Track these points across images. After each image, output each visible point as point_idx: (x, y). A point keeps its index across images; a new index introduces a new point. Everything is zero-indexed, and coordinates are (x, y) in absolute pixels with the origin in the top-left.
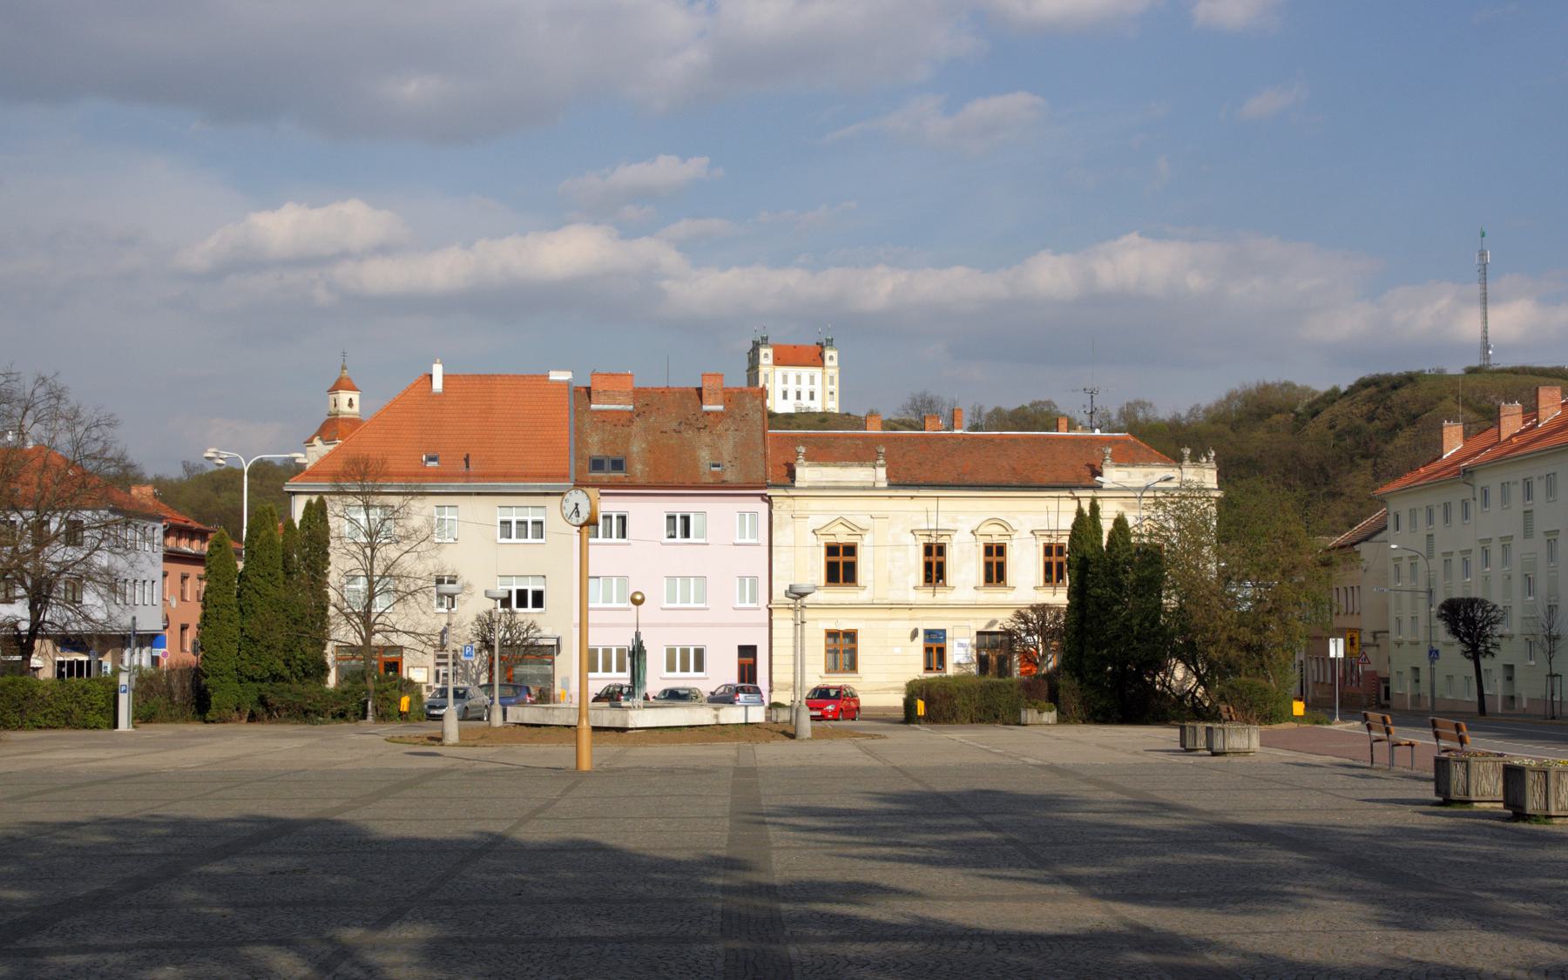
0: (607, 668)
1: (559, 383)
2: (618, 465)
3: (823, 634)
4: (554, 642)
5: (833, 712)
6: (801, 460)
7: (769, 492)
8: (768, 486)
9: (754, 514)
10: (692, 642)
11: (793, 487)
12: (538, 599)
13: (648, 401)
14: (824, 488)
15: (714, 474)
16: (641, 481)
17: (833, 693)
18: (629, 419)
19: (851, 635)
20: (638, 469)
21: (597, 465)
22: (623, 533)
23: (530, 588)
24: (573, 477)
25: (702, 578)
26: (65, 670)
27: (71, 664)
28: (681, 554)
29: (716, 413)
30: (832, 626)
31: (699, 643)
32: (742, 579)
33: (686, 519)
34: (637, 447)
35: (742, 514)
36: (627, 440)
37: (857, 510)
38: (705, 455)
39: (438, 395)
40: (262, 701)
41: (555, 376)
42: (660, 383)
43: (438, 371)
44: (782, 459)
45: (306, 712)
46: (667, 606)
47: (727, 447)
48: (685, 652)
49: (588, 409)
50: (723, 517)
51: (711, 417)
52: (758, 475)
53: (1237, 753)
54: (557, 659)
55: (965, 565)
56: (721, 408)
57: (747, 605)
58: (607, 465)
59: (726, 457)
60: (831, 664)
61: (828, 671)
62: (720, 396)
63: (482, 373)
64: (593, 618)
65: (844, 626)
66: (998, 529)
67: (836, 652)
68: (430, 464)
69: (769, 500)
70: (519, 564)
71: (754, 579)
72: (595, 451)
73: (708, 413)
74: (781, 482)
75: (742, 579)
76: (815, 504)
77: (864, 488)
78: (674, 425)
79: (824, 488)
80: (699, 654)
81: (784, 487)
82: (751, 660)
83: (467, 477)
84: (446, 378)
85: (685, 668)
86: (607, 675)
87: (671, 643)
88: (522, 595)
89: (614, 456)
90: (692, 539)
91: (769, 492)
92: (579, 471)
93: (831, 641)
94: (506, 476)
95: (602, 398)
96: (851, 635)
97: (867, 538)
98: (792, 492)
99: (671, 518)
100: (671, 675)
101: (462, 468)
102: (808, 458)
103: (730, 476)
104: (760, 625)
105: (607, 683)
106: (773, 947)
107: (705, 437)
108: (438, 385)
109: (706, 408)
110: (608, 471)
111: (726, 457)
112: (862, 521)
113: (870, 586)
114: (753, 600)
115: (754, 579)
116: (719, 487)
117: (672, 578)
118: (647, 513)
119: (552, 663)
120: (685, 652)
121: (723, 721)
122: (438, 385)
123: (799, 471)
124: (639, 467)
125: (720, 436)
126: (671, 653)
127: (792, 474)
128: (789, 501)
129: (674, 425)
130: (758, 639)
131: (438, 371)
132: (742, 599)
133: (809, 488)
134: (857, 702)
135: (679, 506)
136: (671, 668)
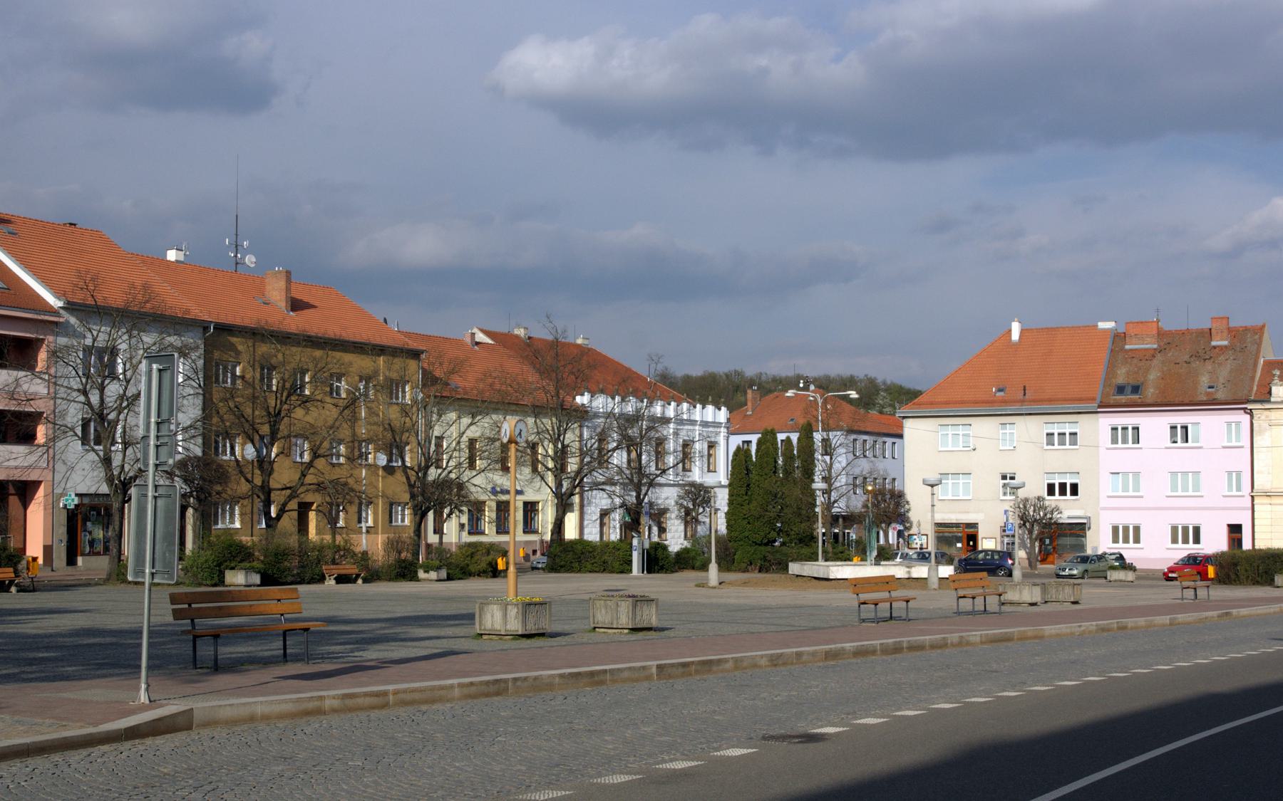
1: (1105, 331)
2: (1136, 389)
6: (1276, 380)
7: (1250, 406)
8: (1248, 401)
9: (1238, 423)
11: (1269, 401)
12: (1075, 489)
13: (1168, 340)
16: (1149, 401)
18: (1153, 354)
20: (1150, 392)
21: (1121, 390)
22: (1137, 440)
23: (1069, 481)
24: (1098, 400)
25: (1197, 473)
28: (1182, 458)
29: (1221, 348)
31: (1136, 522)
32: (1230, 473)
33: (1185, 428)
34: (1153, 376)
35: (1229, 424)
36: (1147, 370)
38: (1205, 380)
39: (1016, 344)
40: (765, 559)
41: (1103, 325)
42: (1184, 328)
43: (1016, 329)
47: (1224, 373)
48: (1185, 529)
52: (1241, 395)
53: (1012, 603)
54: (1088, 533)
56: (1225, 343)
58: (1129, 389)
59: (1221, 380)
62: (1225, 334)
63: (1049, 326)
69: (1250, 413)
70: (1061, 463)
71: (1239, 474)
72: (1120, 380)
73: (1214, 347)
75: (1230, 473)
78: (1186, 358)
80: (1197, 530)
81: (1261, 402)
83: (1022, 402)
84: (1022, 332)
85: (1186, 541)
86: (1186, 546)
87: (1116, 522)
88: (1063, 486)
89: (1132, 382)
90: (1190, 444)
92: (1104, 395)
94: (1050, 401)
99: (1173, 428)
100: (1175, 546)
101: (1020, 396)
103: (1220, 395)
106: (143, 686)
108: (1015, 336)
109: (1214, 343)
110: (1127, 395)
111: (1221, 380)
114: (1239, 489)
115: (1239, 474)
116: (1211, 403)
117: (1174, 474)
118: (1155, 425)
121: (915, 575)
122: (1015, 336)
123: (1274, 389)
125: (1220, 364)
126: (1115, 529)
128: (1267, 413)
129: (1186, 358)
130: (1243, 519)
131: (1016, 329)
132: (1230, 488)
135: (1179, 419)
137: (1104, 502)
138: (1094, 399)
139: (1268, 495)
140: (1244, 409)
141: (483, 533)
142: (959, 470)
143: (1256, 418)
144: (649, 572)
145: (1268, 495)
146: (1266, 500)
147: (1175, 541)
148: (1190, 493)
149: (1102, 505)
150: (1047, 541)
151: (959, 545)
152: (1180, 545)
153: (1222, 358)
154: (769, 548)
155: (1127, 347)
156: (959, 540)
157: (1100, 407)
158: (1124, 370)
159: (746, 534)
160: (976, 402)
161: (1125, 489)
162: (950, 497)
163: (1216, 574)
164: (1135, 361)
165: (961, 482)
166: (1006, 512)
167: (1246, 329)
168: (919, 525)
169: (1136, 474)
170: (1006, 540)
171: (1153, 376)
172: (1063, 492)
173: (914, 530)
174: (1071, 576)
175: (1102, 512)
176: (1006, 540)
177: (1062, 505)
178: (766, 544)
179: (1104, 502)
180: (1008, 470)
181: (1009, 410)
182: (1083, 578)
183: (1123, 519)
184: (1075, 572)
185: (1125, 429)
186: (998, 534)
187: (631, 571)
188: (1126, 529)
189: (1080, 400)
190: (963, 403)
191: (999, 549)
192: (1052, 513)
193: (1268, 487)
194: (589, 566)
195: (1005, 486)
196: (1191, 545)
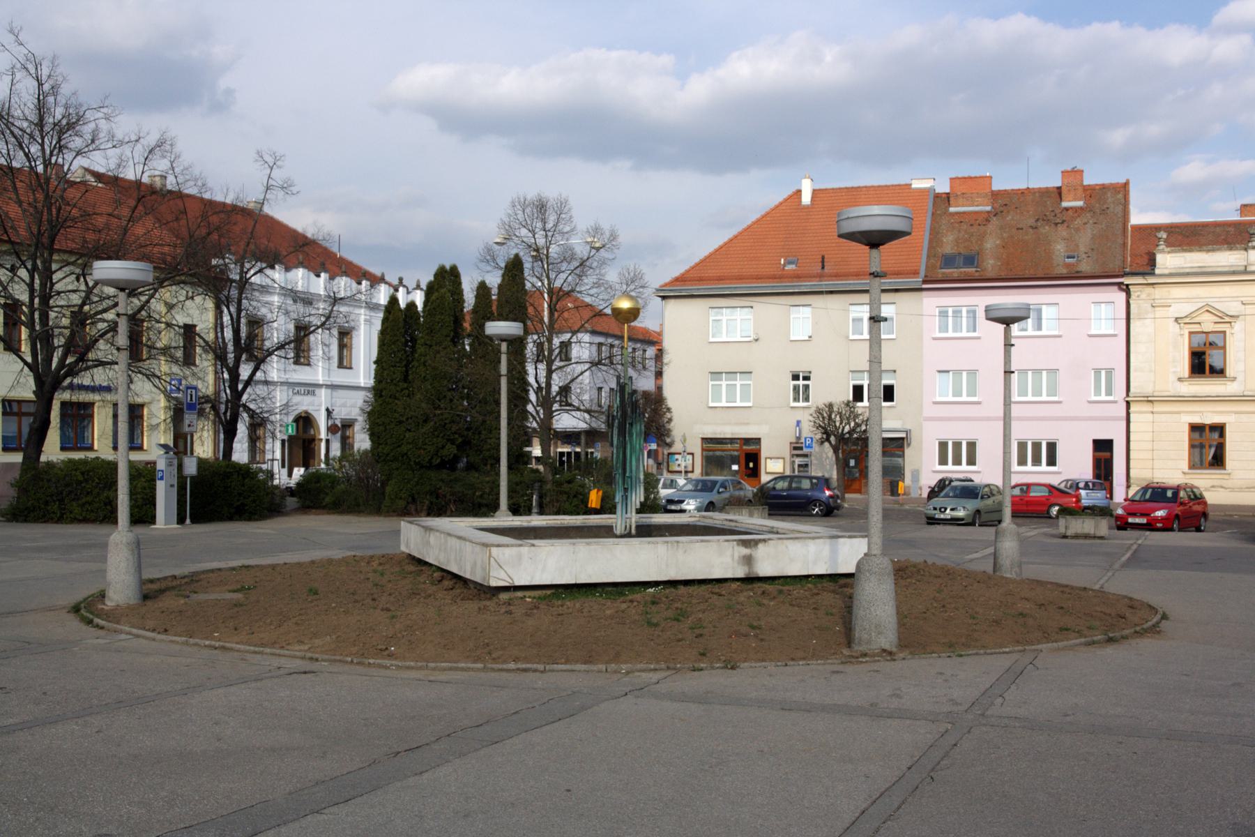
0: (957, 462)
2: (970, 260)
3: (1186, 429)
4: (903, 435)
5: (1163, 519)
7: (1127, 281)
8: (1125, 275)
10: (1044, 436)
11: (1152, 274)
12: (889, 393)
14: (1188, 274)
15: (1068, 265)
16: (990, 275)
17: (1169, 494)
18: (987, 218)
19: (1220, 429)
20: (990, 264)
21: (949, 261)
24: (922, 273)
25: (1053, 372)
26: (565, 459)
27: (569, 454)
30: (1197, 420)
31: (1051, 437)
32: (1097, 372)
34: (990, 244)
36: (982, 237)
37: (1226, 297)
38: (1060, 248)
39: (807, 207)
40: (435, 493)
42: (1024, 187)
44: (1143, 249)
45: (480, 505)
46: (1094, 398)
47: (1084, 240)
49: (946, 212)
50: (1097, 309)
51: (1070, 212)
52: (1114, 265)
54: (907, 452)
56: (1080, 203)
57: (1103, 397)
59: (1082, 249)
60: (1197, 460)
61: (1192, 466)
64: (1015, 411)
65: (1210, 419)
67: (1202, 446)
68: (789, 267)
69: (1127, 289)
71: (1110, 372)
73: (1067, 209)
74: (1141, 270)
76: (1178, 292)
77: (1234, 273)
78: (1031, 222)
79: (1188, 274)
80: (1052, 447)
81: (1143, 274)
82: (1107, 454)
83: (820, 277)
84: (815, 193)
87: (943, 437)
91: (1127, 281)
93: (1197, 435)
95: (961, 201)
96: (1220, 429)
97: (1238, 326)
98: (1151, 280)
102: (1169, 243)
103: (1085, 267)
104: (995, 419)
105: (940, 476)
107: (1063, 231)
109: (1065, 204)
111: (1082, 249)
112: (1233, 308)
113: (1240, 378)
114: (1109, 393)
116: (1073, 278)
119: (903, 456)
120: (1037, 446)
121: (765, 568)
123: (1160, 258)
124: (991, 262)
125: (1077, 230)
126: (943, 446)
127: (1152, 262)
128: (1149, 290)
129: (1031, 222)
130: (1115, 433)
132: (1098, 392)
133: (1171, 275)
134: (1205, 503)
136: (943, 461)
137: (929, 411)
139: (1149, 400)
140: (1119, 284)
141: (91, 448)
142: (740, 371)
143: (1134, 295)
144: (195, 520)
145: (1149, 400)
146: (1147, 407)
148: (1044, 398)
150: (852, 463)
151: (735, 467)
153: (1078, 222)
154: (444, 474)
155: (952, 209)
156: (734, 460)
157: (925, 282)
159: (404, 448)
160: (758, 278)
161: (957, 392)
162: (724, 404)
164: (964, 227)
165: (738, 383)
166: (798, 423)
167: (1104, 187)
168: (684, 440)
169: (972, 373)
170: (798, 461)
171: (990, 244)
173: (677, 447)
174: (955, 521)
175: (926, 425)
176: (798, 461)
178: (441, 466)
179: (929, 411)
180: (801, 368)
181: (806, 285)
182: (972, 524)
183: (952, 433)
184: (961, 513)
185: (957, 313)
186: (787, 452)
187: (152, 520)
188: (957, 445)
190: (740, 278)
191: (788, 473)
193: (1148, 389)
194: (77, 510)
195: (796, 388)
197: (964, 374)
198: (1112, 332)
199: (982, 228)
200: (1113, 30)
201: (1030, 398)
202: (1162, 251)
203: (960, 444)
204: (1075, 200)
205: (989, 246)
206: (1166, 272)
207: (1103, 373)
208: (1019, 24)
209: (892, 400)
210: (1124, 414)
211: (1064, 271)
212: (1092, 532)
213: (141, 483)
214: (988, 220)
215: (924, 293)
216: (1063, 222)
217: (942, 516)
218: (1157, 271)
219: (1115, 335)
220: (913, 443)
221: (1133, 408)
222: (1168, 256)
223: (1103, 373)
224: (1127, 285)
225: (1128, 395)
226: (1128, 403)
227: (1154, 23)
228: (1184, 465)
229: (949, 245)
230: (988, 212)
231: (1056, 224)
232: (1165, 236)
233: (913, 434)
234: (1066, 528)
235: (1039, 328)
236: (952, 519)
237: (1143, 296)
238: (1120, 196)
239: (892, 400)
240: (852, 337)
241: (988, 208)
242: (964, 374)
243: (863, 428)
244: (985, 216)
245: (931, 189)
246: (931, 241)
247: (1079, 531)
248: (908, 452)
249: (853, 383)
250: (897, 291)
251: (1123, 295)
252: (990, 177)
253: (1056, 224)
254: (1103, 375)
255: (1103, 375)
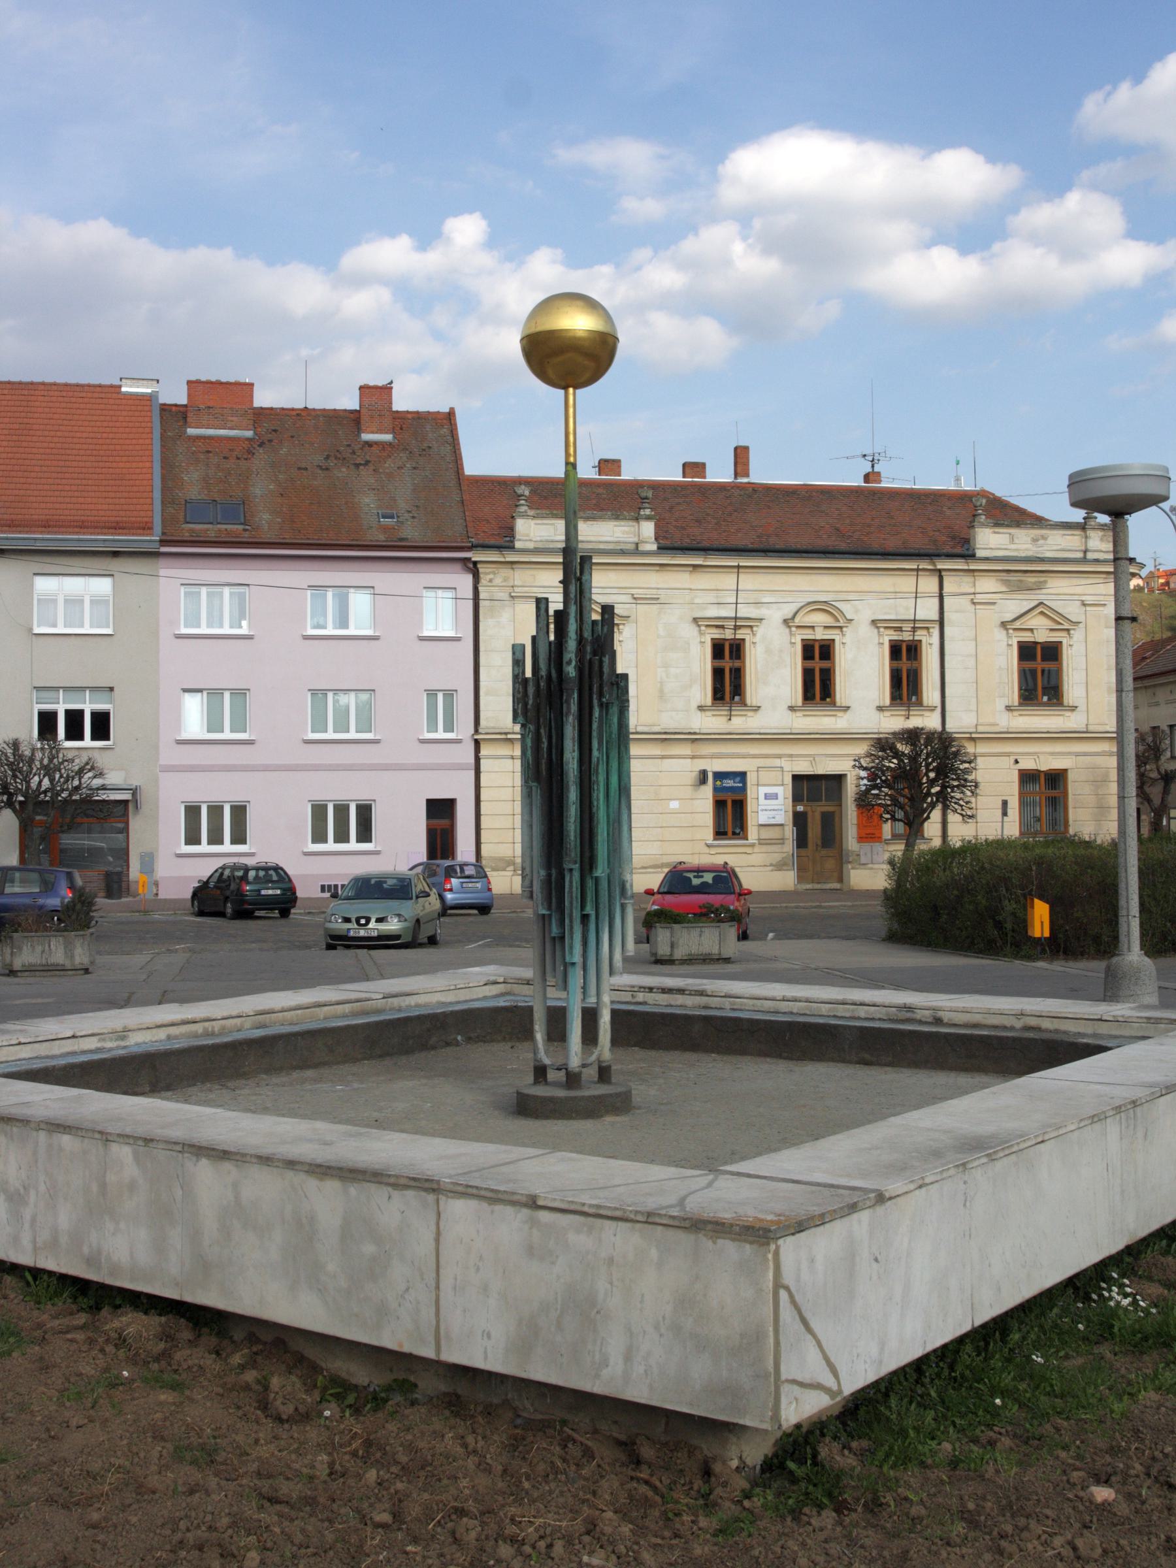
0: (342, 837)
11: (511, 547)
15: (385, 529)
18: (249, 449)
20: (265, 520)
23: (88, 707)
31: (364, 796)
32: (432, 694)
34: (261, 488)
38: (368, 502)
42: (302, 406)
47: (403, 492)
48: (341, 811)
49: (181, 434)
51: (375, 449)
55: (774, 675)
56: (388, 437)
57: (441, 735)
59: (402, 505)
66: (820, 619)
69: (473, 569)
71: (450, 695)
73: (369, 444)
77: (623, 552)
78: (318, 459)
80: (365, 812)
81: (499, 548)
87: (193, 797)
98: (511, 557)
103: (411, 532)
105: (218, 863)
109: (366, 437)
111: (402, 505)
114: (449, 728)
115: (450, 695)
119: (126, 830)
124: (266, 516)
126: (192, 812)
127: (510, 532)
128: (505, 572)
129: (318, 459)
130: (459, 788)
132: (433, 727)
133: (536, 551)
137: (169, 755)
138: (147, 528)
143: (484, 580)
146: (656, 750)
147: (319, 836)
149: (164, 760)
152: (204, 847)
153: (389, 464)
155: (191, 431)
157: (163, 542)
158: (196, 475)
161: (214, 723)
163: (1026, 906)
169: (240, 694)
172: (75, 731)
177: (101, 760)
179: (169, 755)
184: (393, 926)
188: (216, 811)
189: (117, 527)
192: (80, 772)
196: (227, 847)
197: (227, 695)
198: (452, 634)
199: (242, 463)
200: (223, 259)
201: (330, 735)
202: (524, 515)
203: (347, 807)
204: (380, 431)
205: (258, 492)
206: (531, 546)
207: (440, 696)
208: (98, 234)
209: (106, 737)
210: (472, 760)
211: (381, 538)
212: (715, 951)
213: (727, 664)
214: (250, 452)
215: (162, 561)
216: (367, 463)
217: (362, 933)
218: (518, 545)
219: (458, 639)
220: (145, 808)
221: (484, 752)
222: (532, 523)
223: (440, 696)
224: (475, 563)
225: (476, 731)
226: (477, 743)
227: (273, 259)
228: (708, 834)
229: (193, 484)
230: (248, 439)
231: (357, 466)
232: (527, 493)
233: (143, 798)
234: (672, 946)
235: (343, 622)
236: (380, 937)
237: (498, 581)
238: (445, 431)
239: (106, 737)
240: (36, 631)
241: (249, 434)
242: (227, 695)
243: (76, 783)
244: (246, 445)
245: (149, 399)
246: (164, 479)
247: (695, 950)
248: (136, 824)
249: (37, 707)
250: (116, 554)
251: (469, 578)
252: (252, 385)
253: (357, 466)
254: (440, 701)
255: (440, 701)
